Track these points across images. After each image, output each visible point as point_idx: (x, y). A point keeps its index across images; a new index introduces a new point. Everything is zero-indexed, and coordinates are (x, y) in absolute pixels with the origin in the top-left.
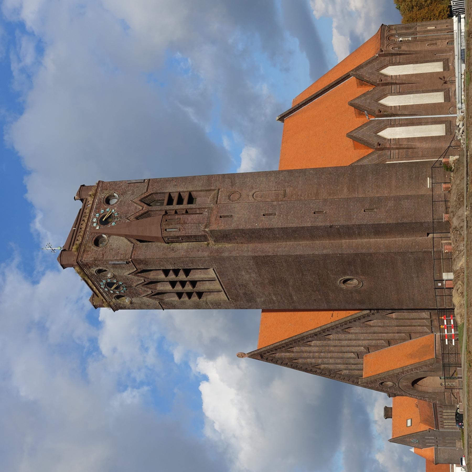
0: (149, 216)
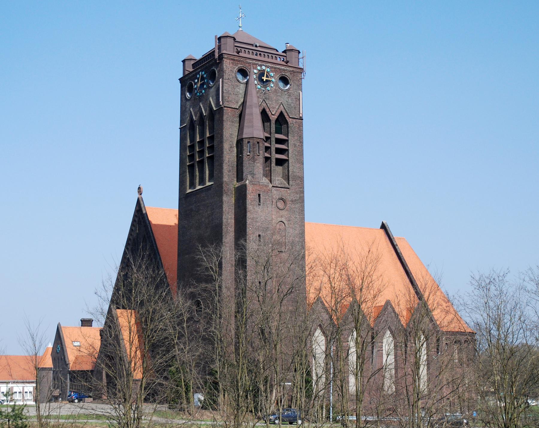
0: (264, 121)
